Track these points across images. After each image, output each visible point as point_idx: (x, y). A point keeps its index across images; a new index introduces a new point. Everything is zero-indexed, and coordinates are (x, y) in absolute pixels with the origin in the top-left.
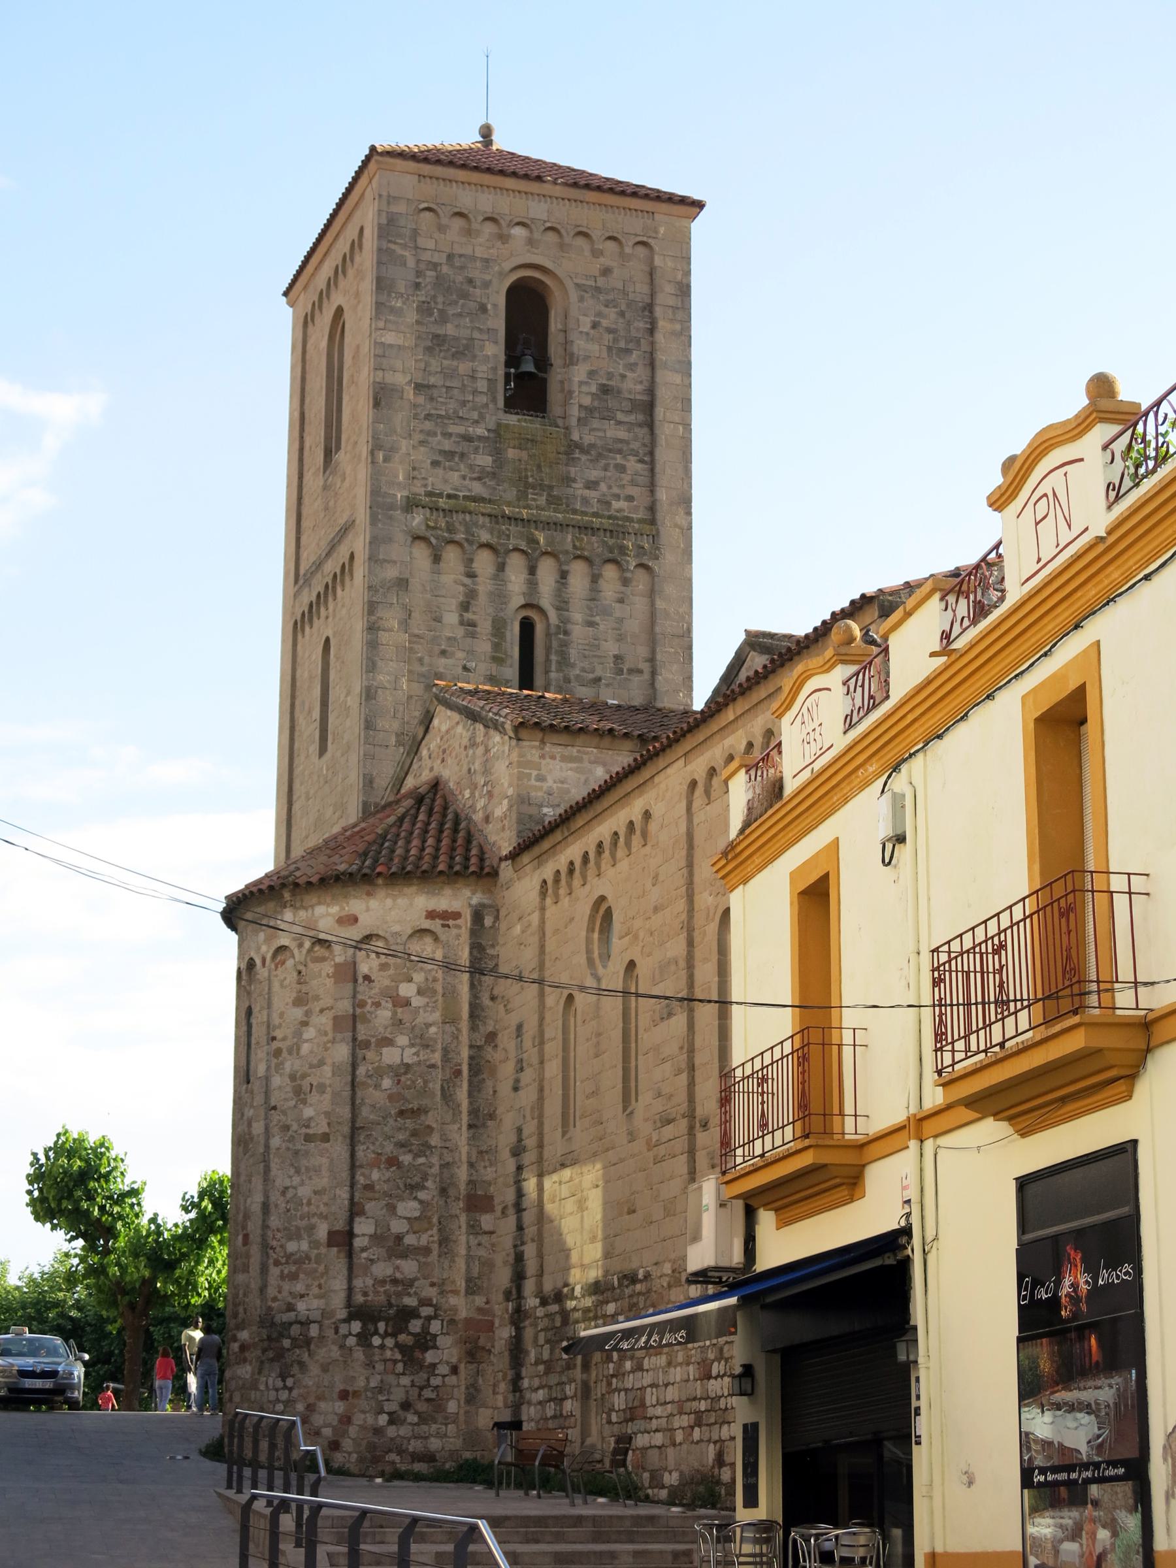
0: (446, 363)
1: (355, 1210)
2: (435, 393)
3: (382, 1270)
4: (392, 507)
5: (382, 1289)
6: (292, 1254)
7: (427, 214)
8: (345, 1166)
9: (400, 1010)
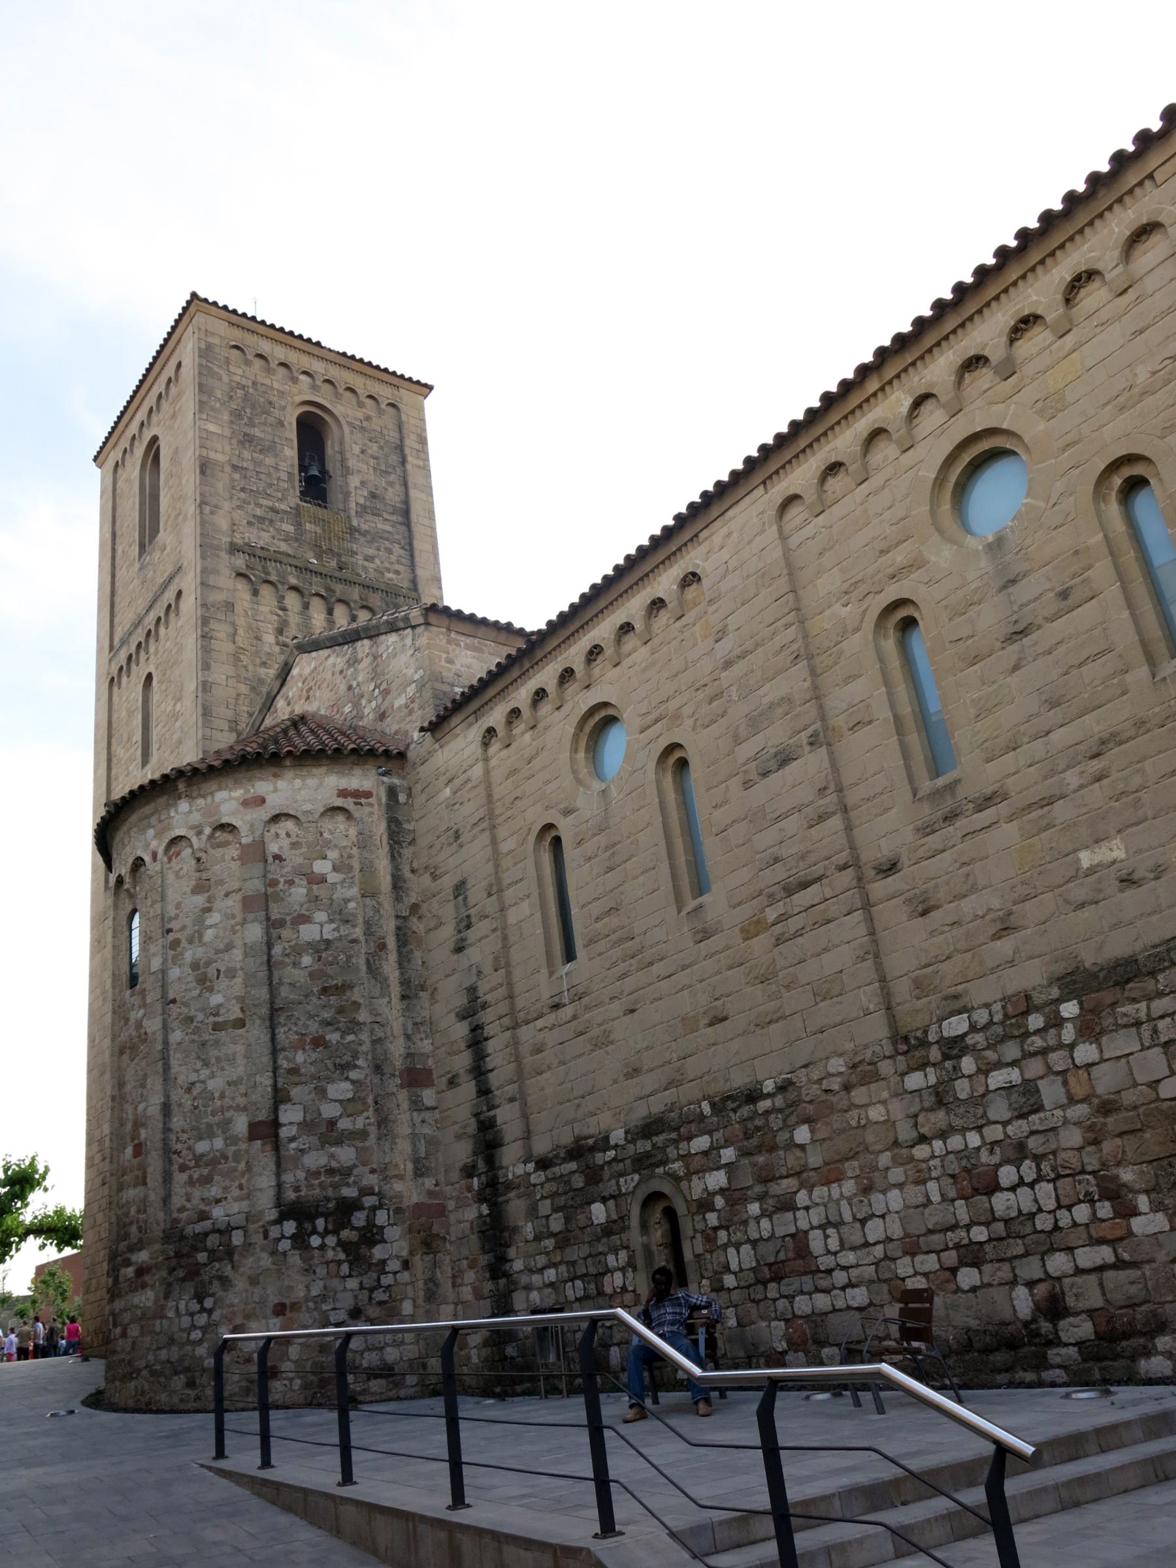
0: (255, 455)
1: (279, 1097)
2: (248, 474)
3: (315, 1160)
4: (218, 548)
5: (317, 1182)
6: (203, 1155)
7: (236, 351)
8: (266, 1050)
9: (315, 887)
